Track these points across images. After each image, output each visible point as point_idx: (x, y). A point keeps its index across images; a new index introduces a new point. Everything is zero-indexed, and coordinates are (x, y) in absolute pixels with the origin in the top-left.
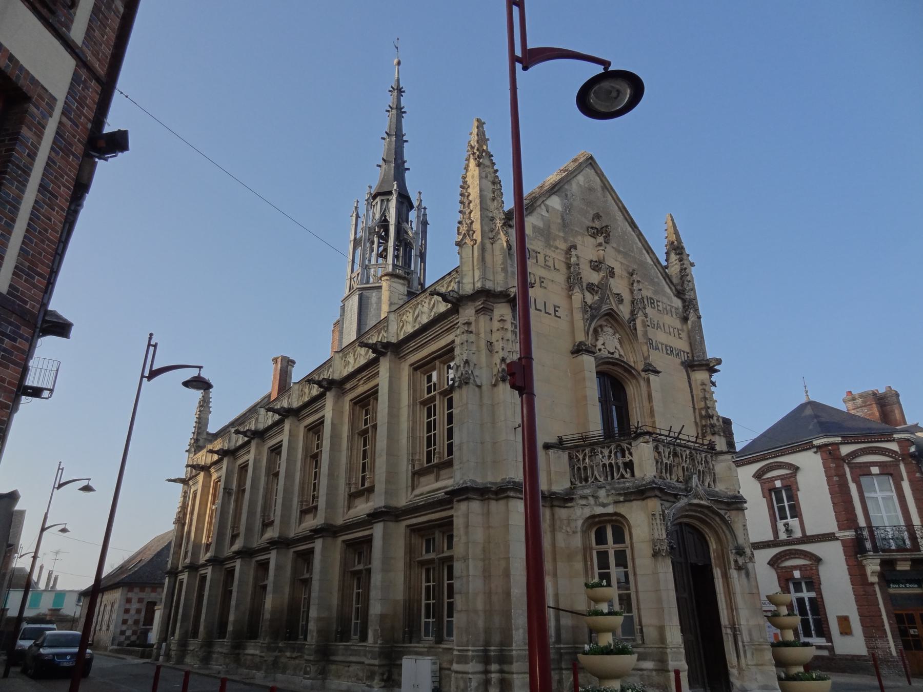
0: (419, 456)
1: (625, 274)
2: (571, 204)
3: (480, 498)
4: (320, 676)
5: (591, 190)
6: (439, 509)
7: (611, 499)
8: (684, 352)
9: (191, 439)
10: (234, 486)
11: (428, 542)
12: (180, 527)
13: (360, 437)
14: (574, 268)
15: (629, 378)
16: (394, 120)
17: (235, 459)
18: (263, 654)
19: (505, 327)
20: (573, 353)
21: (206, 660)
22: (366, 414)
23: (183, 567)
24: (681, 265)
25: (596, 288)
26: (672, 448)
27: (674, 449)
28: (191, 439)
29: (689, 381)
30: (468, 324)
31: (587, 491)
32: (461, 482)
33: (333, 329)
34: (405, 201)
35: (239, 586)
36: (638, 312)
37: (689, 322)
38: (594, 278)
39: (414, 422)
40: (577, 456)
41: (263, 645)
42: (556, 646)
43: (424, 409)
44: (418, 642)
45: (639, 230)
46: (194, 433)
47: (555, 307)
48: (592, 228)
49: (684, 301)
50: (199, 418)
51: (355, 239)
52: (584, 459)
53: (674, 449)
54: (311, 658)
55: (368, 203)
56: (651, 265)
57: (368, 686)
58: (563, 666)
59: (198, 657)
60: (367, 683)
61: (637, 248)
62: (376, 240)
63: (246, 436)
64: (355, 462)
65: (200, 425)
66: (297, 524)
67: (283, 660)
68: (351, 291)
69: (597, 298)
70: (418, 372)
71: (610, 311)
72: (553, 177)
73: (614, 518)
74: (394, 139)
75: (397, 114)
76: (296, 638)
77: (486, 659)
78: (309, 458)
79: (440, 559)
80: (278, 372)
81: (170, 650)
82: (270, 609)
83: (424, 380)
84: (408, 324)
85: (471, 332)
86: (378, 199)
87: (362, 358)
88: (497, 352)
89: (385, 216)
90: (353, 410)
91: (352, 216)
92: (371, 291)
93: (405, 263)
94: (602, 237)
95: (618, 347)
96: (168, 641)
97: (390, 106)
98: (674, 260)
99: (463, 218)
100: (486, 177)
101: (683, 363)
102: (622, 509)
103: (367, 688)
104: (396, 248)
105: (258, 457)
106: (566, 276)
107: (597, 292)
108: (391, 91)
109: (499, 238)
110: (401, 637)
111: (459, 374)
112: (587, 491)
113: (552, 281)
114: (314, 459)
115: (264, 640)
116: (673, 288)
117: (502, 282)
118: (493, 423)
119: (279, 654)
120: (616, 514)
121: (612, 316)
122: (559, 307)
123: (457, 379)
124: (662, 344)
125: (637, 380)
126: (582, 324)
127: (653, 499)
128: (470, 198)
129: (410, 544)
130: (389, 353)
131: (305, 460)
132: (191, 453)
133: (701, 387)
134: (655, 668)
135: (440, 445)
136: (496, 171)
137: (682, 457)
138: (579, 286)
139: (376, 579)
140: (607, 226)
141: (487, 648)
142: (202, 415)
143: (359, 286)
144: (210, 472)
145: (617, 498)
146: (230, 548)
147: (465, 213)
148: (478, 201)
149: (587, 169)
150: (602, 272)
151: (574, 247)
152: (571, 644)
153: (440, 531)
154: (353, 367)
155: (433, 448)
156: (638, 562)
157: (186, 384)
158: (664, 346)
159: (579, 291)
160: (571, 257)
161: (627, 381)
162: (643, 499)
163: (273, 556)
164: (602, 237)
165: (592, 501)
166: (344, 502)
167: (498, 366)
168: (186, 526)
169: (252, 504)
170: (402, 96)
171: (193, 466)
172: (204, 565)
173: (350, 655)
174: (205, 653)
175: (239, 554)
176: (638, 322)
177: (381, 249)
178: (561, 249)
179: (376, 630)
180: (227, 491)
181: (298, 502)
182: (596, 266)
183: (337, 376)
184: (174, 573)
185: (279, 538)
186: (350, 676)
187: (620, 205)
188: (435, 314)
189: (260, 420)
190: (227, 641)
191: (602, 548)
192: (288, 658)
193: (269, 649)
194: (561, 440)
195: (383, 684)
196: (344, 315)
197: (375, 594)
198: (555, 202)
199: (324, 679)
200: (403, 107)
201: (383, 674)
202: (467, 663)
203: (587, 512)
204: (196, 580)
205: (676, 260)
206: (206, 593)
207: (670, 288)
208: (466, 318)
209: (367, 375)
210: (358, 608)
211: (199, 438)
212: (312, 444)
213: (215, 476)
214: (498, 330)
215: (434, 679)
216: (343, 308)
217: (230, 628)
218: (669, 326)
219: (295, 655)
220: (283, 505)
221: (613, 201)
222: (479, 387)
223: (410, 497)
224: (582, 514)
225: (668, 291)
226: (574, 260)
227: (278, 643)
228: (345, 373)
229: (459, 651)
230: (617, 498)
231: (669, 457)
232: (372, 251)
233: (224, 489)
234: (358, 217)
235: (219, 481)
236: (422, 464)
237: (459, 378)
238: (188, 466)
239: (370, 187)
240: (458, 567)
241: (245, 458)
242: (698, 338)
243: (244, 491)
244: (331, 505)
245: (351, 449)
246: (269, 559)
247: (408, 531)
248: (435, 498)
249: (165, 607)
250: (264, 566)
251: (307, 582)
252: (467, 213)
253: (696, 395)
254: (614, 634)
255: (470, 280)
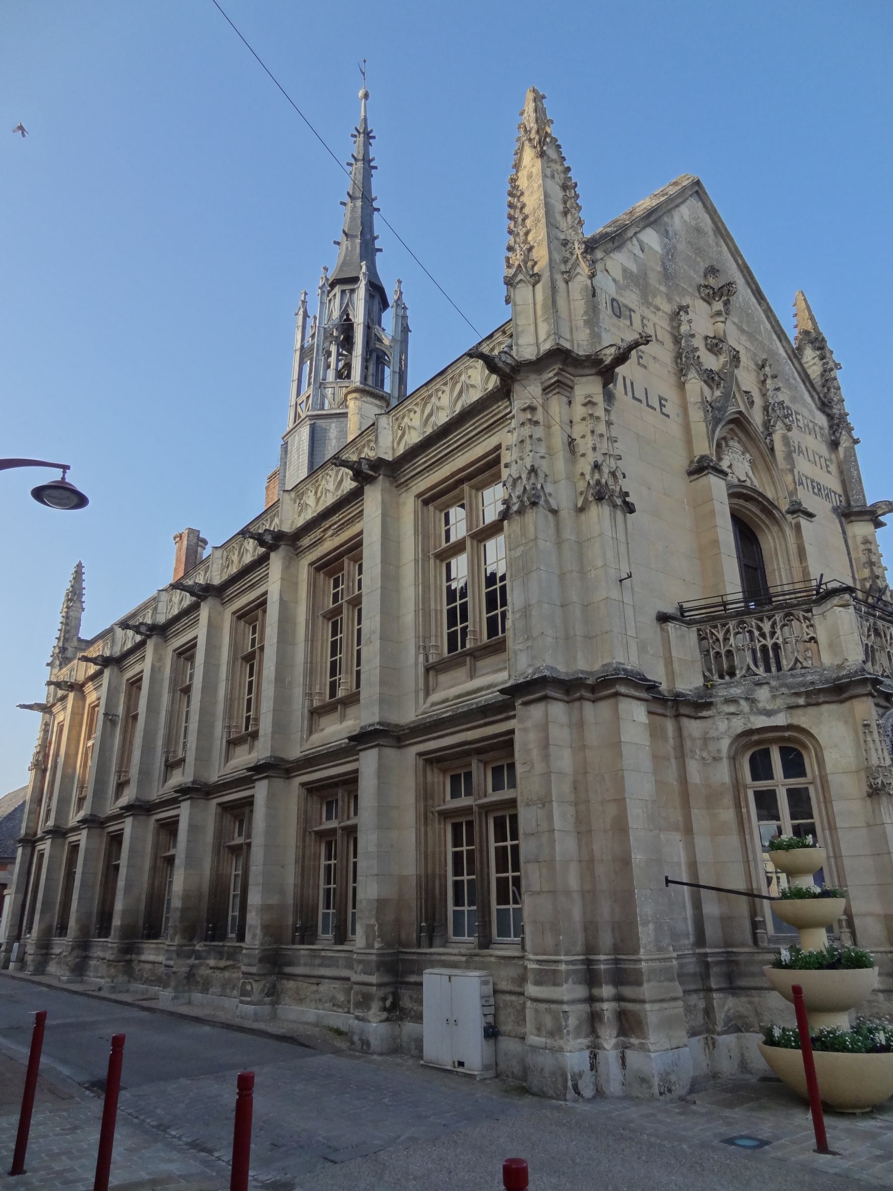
0: (436, 641)
1: (752, 366)
2: (675, 247)
3: (566, 698)
4: (269, 999)
5: (698, 230)
6: (482, 722)
7: (780, 703)
8: (835, 493)
9: (54, 647)
10: (121, 710)
11: (455, 780)
12: (39, 777)
13: (326, 621)
14: (686, 342)
15: (767, 522)
16: (360, 177)
17: (122, 670)
18: (171, 963)
19: (596, 414)
20: (690, 473)
21: (80, 969)
22: (336, 585)
23: (43, 832)
24: (824, 364)
25: (717, 378)
26: (872, 620)
27: (875, 624)
28: (54, 647)
29: (844, 537)
30: (532, 409)
31: (736, 691)
32: (530, 671)
33: (266, 484)
34: (376, 292)
35: (130, 857)
36: (776, 423)
37: (841, 449)
38: (712, 362)
39: (426, 587)
40: (712, 634)
41: (172, 948)
42: (697, 951)
43: (441, 567)
44: (444, 946)
45: (768, 304)
46: (59, 639)
47: (661, 399)
48: (706, 286)
49: (830, 417)
50: (67, 617)
51: (302, 347)
52: (726, 639)
53: (875, 624)
54: (254, 970)
55: (323, 292)
56: (785, 358)
57: (357, 1018)
58: (714, 986)
59: (67, 965)
60: (357, 1014)
61: (766, 329)
62: (333, 349)
63: (138, 632)
64: (319, 660)
65: (68, 628)
66: (223, 760)
67: (204, 971)
68: (297, 422)
69: (718, 393)
70: (431, 507)
71: (737, 416)
72: (646, 203)
73: (787, 734)
74: (359, 203)
75: (364, 168)
76: (223, 937)
77: (591, 978)
78: (240, 660)
79: (481, 807)
80: (184, 551)
81: (25, 953)
82: (181, 893)
83: (440, 521)
84: (412, 430)
85: (536, 423)
86: (337, 290)
87: (329, 495)
88: (583, 455)
89: (348, 315)
90: (315, 579)
91: (297, 314)
92: (330, 420)
93: (376, 381)
94: (721, 303)
95: (751, 474)
96: (22, 941)
97: (353, 156)
98: (810, 358)
99: (515, 242)
100: (553, 177)
101: (835, 510)
102: (803, 719)
103: (356, 1022)
104: (366, 361)
105: (157, 665)
106: (673, 355)
107: (718, 385)
108: (354, 136)
109: (578, 274)
110: (415, 935)
111: (519, 490)
112: (736, 691)
113: (655, 358)
114: (247, 662)
115: (172, 939)
116: (816, 397)
117: (585, 343)
118: (582, 572)
119: (197, 962)
120: (790, 727)
121: (740, 422)
122: (666, 401)
123: (515, 500)
124: (807, 478)
125: (781, 529)
126: (705, 429)
127: (865, 699)
128: (526, 211)
129: (425, 783)
130: (381, 477)
131: (234, 662)
132: (55, 668)
133: (862, 547)
134: (881, 987)
135: (474, 620)
136: (568, 169)
137: (885, 636)
138: (696, 369)
139: (368, 840)
140: (730, 284)
141: (592, 957)
142: (71, 613)
143: (309, 413)
144: (83, 692)
145: (793, 701)
146: (114, 803)
147: (518, 234)
148: (541, 212)
149: (692, 199)
150: (724, 355)
151: (684, 309)
152: (720, 947)
153: (480, 761)
154: (314, 511)
155: (459, 627)
156: (838, 806)
157: (39, 494)
158: (809, 481)
159: (697, 376)
160: (680, 325)
161: (766, 530)
162: (842, 702)
163: (184, 811)
164: (721, 303)
165: (745, 706)
166: (303, 722)
167: (588, 477)
168: (48, 773)
169: (149, 736)
170: (370, 144)
171: (58, 685)
172: (74, 829)
173: (320, 965)
174: (78, 960)
175: (130, 809)
176: (777, 437)
177: (341, 364)
178: (663, 312)
179: (369, 927)
180: (110, 718)
181: (224, 727)
182: (715, 345)
183: (287, 528)
184: (30, 842)
185: (193, 782)
186: (320, 1000)
187: (740, 262)
188: (463, 406)
189: (159, 610)
190: (113, 940)
191: (764, 785)
192: (211, 968)
193: (180, 954)
194: (682, 610)
195: (385, 1015)
196: (286, 458)
197: (366, 864)
198: (651, 237)
199: (274, 1003)
200: (373, 159)
201: (384, 999)
202: (556, 984)
203: (739, 725)
204: (63, 850)
205: (814, 358)
206: (79, 870)
207: (812, 397)
208: (527, 401)
209: (340, 520)
210: (329, 889)
211: (66, 646)
212: (244, 639)
213: (91, 698)
214: (584, 419)
215: (488, 1010)
216: (285, 448)
217: (116, 922)
218: (813, 451)
219: (223, 964)
220: (200, 731)
221: (729, 255)
222: (555, 512)
223: (423, 707)
224: (729, 728)
225: (809, 399)
226: (684, 329)
227: (194, 946)
228: (300, 522)
229: (539, 962)
230: (793, 701)
231: (869, 636)
232: (329, 367)
233: (106, 714)
234: (306, 315)
235: (97, 706)
236: (441, 654)
237: (518, 497)
238: (49, 683)
239: (326, 269)
240: (527, 818)
241: (137, 668)
242: (855, 473)
243: (135, 718)
244: (280, 727)
245: (312, 641)
246: (178, 816)
247: (421, 762)
248: (472, 704)
249: (17, 891)
250: (170, 827)
251: (241, 851)
252: (521, 234)
253: (855, 559)
254: (830, 929)
255: (532, 340)
